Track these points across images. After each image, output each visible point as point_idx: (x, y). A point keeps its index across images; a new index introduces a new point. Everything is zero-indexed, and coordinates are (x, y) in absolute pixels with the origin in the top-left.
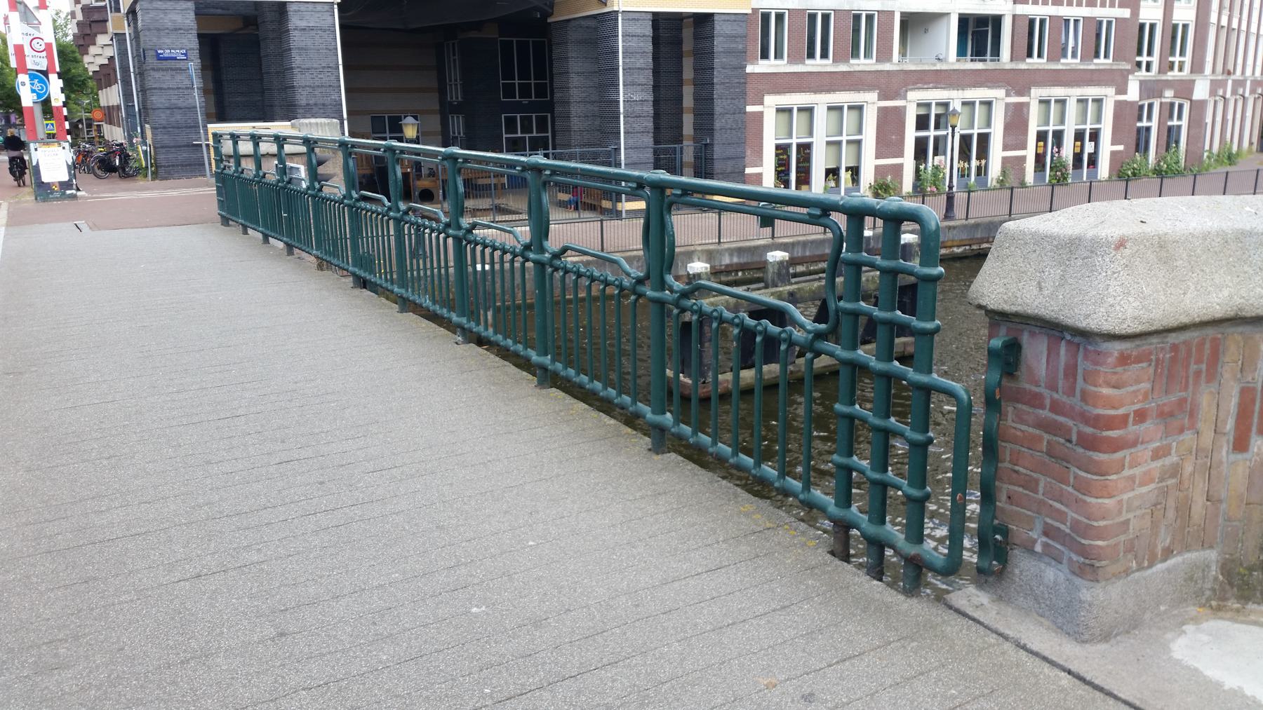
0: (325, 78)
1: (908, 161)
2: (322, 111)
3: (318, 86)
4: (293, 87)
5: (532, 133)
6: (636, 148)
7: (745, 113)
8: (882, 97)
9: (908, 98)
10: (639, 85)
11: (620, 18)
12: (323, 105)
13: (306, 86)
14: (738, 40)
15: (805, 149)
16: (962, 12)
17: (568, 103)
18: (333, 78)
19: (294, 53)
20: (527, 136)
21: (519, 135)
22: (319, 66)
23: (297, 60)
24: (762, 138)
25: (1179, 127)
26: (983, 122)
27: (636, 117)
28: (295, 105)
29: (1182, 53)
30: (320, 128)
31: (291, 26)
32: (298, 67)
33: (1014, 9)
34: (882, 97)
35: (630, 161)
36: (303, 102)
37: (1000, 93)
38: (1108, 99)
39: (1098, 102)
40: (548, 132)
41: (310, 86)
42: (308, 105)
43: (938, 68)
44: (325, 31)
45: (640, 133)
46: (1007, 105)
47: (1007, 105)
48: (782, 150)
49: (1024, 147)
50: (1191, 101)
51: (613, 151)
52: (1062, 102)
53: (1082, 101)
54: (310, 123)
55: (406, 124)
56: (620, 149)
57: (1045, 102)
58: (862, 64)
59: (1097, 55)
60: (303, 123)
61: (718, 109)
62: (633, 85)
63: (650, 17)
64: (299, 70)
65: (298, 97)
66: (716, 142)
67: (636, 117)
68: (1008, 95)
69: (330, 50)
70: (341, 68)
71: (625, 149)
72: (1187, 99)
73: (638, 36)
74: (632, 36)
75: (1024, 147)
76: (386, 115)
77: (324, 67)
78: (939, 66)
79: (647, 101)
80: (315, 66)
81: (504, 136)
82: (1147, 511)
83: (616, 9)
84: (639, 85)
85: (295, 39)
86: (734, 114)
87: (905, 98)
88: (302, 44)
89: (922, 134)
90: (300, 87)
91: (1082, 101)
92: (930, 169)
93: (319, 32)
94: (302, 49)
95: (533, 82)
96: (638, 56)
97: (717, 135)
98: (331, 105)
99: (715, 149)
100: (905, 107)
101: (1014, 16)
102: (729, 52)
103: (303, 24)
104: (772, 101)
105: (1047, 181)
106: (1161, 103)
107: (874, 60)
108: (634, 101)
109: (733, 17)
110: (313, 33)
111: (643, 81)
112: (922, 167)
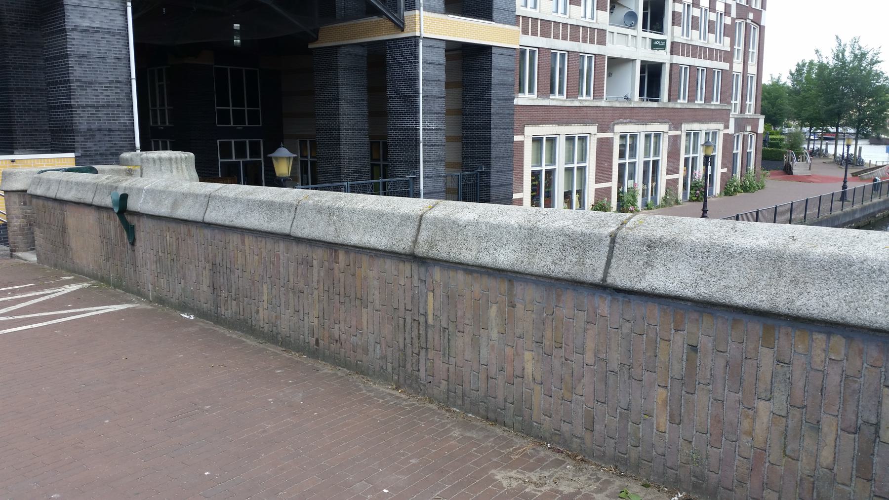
0: (114, 96)
1: (614, 184)
2: (107, 138)
3: (103, 106)
4: (70, 106)
5: (246, 157)
6: (432, 177)
7: (513, 142)
8: (601, 130)
9: (615, 131)
10: (435, 113)
11: (421, 44)
12: (110, 130)
13: (87, 106)
14: (509, 73)
15: (550, 173)
16: (642, 59)
17: (338, 130)
18: (122, 95)
19: (72, 62)
20: (241, 160)
21: (234, 159)
22: (105, 80)
23: (77, 71)
24: (523, 166)
25: (751, 152)
26: (686, 152)
27: (432, 145)
28: (73, 131)
29: (736, 99)
30: (174, 166)
31: (69, 24)
32: (77, 81)
33: (671, 59)
34: (601, 130)
35: (430, 189)
36: (84, 127)
37: (593, 129)
38: (592, 137)
39: (583, 139)
40: (260, 157)
41: (92, 106)
42: (89, 130)
43: (632, 106)
44: (113, 34)
45: (434, 161)
46: (670, 136)
47: (670, 136)
48: (536, 175)
49: (677, 172)
50: (757, 133)
51: (411, 181)
52: (552, 140)
53: (570, 139)
54: (160, 159)
55: (277, 158)
56: (419, 178)
57: (537, 141)
58: (585, 100)
59: (552, 91)
60: (148, 159)
61: (494, 139)
62: (430, 113)
63: (443, 45)
64: (78, 84)
65: (76, 120)
66: (492, 170)
67: (432, 145)
68: (670, 129)
69: (120, 60)
70: (134, 82)
71: (424, 178)
72: (755, 133)
73: (434, 64)
74: (430, 63)
75: (677, 172)
76: (381, 141)
77: (111, 82)
78: (626, 105)
79: (364, 130)
80: (100, 79)
81: (220, 161)
82: (317, 273)
83: (417, 34)
84: (435, 113)
85: (74, 43)
86: (506, 143)
87: (613, 131)
88: (84, 50)
89: (622, 161)
90: (79, 106)
91: (570, 139)
92: (626, 190)
93: (106, 36)
94: (83, 56)
95: (231, 108)
96: (434, 83)
97: (493, 163)
98: (119, 130)
99: (492, 176)
100: (613, 138)
101: (671, 65)
102: (503, 84)
103: (85, 23)
104: (531, 131)
105: (688, 198)
106: (744, 135)
107: (565, 97)
108: (430, 129)
109: (505, 52)
110: (98, 36)
111: (438, 109)
112: (621, 189)
